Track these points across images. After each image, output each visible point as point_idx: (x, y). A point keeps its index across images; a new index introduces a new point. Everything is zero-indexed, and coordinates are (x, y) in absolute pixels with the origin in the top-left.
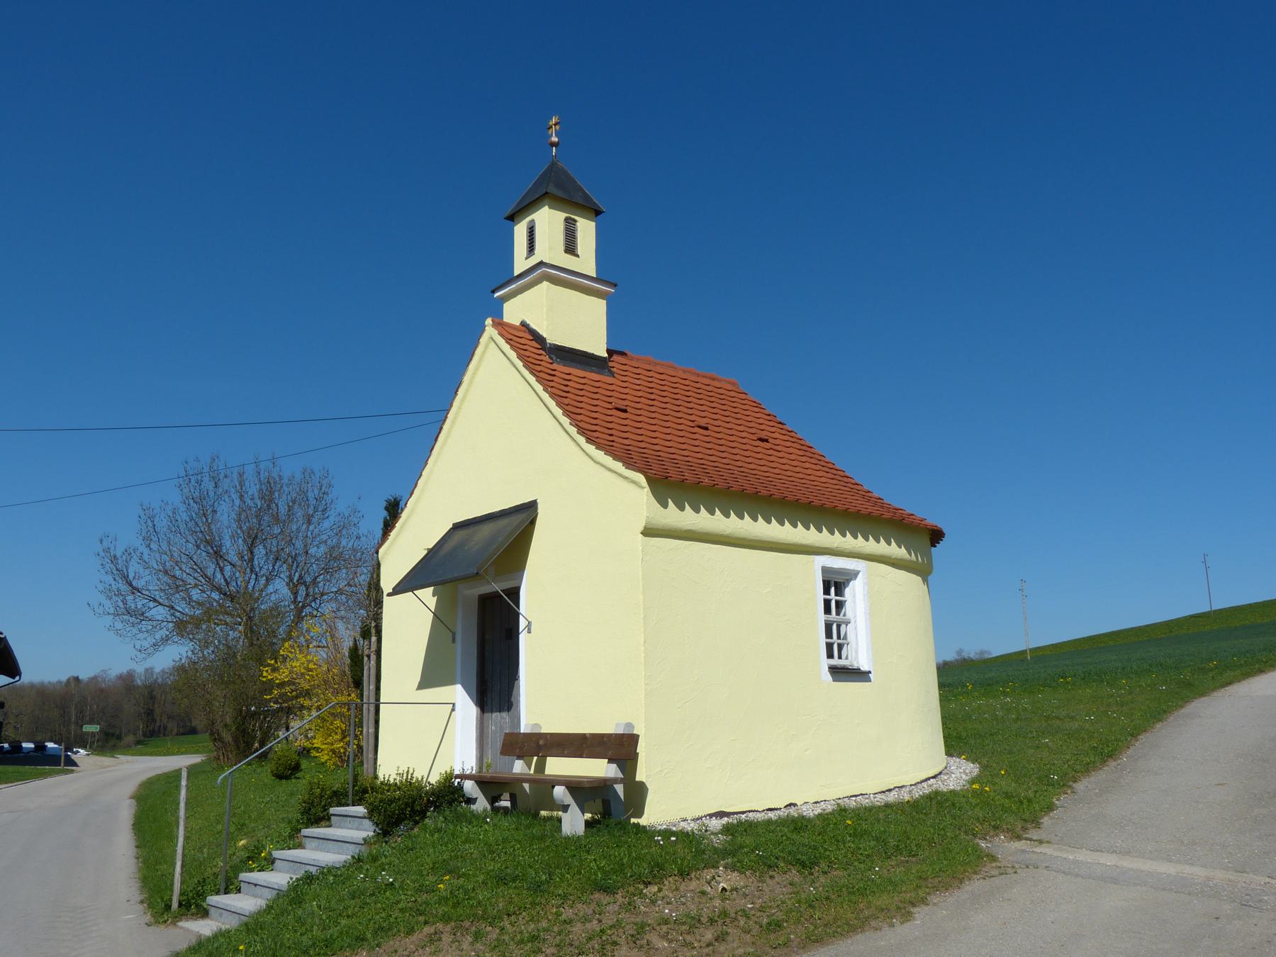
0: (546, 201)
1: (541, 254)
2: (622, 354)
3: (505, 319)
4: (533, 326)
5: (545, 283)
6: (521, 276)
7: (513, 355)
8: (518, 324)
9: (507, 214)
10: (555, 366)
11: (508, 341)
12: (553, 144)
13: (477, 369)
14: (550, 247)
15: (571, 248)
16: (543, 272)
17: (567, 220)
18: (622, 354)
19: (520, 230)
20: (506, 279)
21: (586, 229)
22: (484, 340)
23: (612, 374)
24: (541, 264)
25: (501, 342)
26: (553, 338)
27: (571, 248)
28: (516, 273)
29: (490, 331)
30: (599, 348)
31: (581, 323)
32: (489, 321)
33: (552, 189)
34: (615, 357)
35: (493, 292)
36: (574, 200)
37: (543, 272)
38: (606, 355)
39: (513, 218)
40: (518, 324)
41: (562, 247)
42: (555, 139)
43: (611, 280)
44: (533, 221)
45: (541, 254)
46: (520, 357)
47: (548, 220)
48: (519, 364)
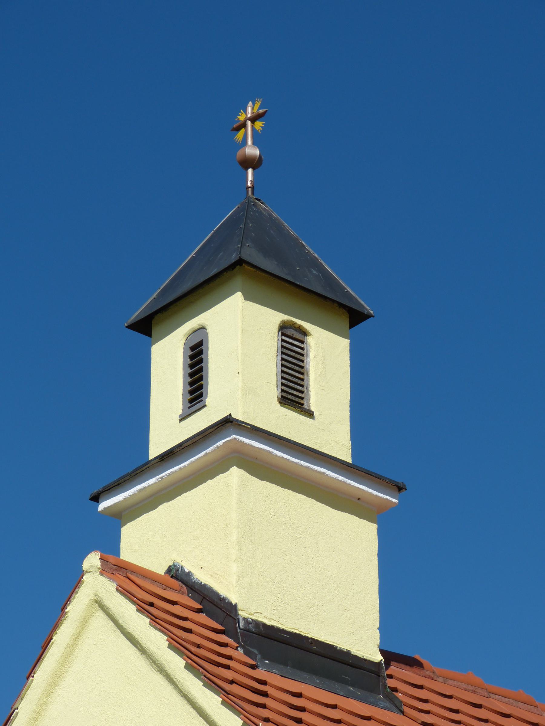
0: (239, 280)
1: (218, 404)
2: (412, 663)
3: (121, 558)
4: (202, 576)
5: (235, 475)
6: (169, 456)
7: (157, 641)
8: (161, 570)
9: (134, 317)
10: (260, 673)
11: (145, 607)
12: (248, 163)
13: (54, 682)
14: (243, 382)
15: (293, 395)
16: (230, 443)
17: (284, 328)
18: (412, 663)
19: (167, 356)
20: (128, 465)
21: (329, 353)
22: (76, 608)
23: (398, 707)
24: (227, 423)
25: (126, 610)
26: (256, 605)
27: (293, 395)
28: (155, 450)
29: (95, 583)
30: (367, 647)
31: (321, 575)
32: (92, 561)
33: (250, 253)
34: (394, 669)
35: (96, 499)
36: (304, 289)
37: (230, 443)
38: (378, 658)
39: (147, 327)
40: (161, 570)
41: (272, 389)
42: (252, 151)
43: (383, 472)
44: (202, 328)
45: (218, 404)
46: (177, 645)
47: (240, 330)
48: (176, 663)
